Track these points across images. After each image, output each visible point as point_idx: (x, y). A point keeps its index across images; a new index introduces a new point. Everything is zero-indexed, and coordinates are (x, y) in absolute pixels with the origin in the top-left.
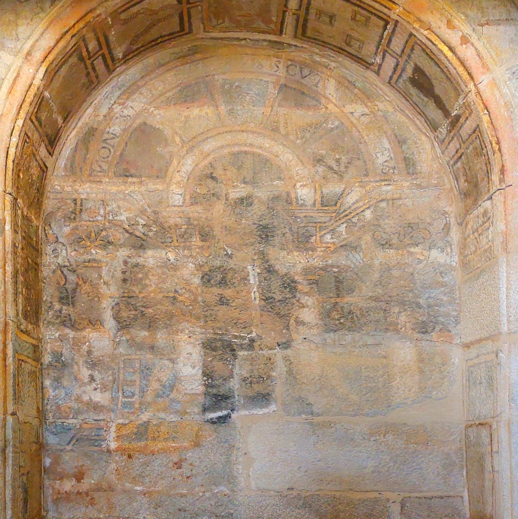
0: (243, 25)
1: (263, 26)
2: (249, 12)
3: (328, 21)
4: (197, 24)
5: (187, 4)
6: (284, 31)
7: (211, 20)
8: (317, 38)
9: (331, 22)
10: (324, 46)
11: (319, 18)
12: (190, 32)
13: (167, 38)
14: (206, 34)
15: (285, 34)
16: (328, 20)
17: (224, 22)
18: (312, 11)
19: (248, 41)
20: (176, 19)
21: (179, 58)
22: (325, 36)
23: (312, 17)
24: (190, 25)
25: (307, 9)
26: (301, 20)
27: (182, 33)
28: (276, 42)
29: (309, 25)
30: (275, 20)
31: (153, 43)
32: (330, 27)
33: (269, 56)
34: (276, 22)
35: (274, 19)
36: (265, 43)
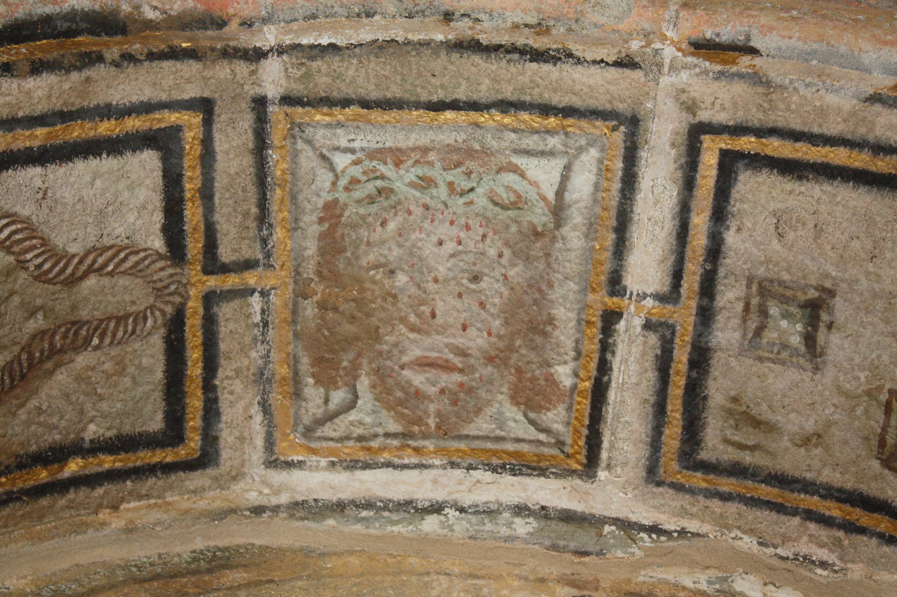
0: (432, 422)
1: (517, 424)
2: (460, 341)
3: (796, 340)
4: (240, 409)
5: (207, 271)
6: (605, 444)
7: (297, 394)
8: (748, 458)
9: (810, 340)
10: (779, 508)
11: (759, 331)
12: (206, 458)
13: (108, 462)
14: (278, 477)
15: (609, 467)
16: (792, 332)
17: (351, 405)
18: (729, 295)
19: (452, 513)
20: (151, 353)
21: (151, 579)
22: (785, 442)
23: (726, 334)
24: (211, 412)
25: (708, 287)
26: (681, 357)
27: (168, 456)
28: (568, 517)
29: (717, 390)
30: (568, 383)
31: (43, 475)
32: (807, 376)
33: (542, 581)
34: (574, 387)
35: (564, 374)
36: (523, 527)
